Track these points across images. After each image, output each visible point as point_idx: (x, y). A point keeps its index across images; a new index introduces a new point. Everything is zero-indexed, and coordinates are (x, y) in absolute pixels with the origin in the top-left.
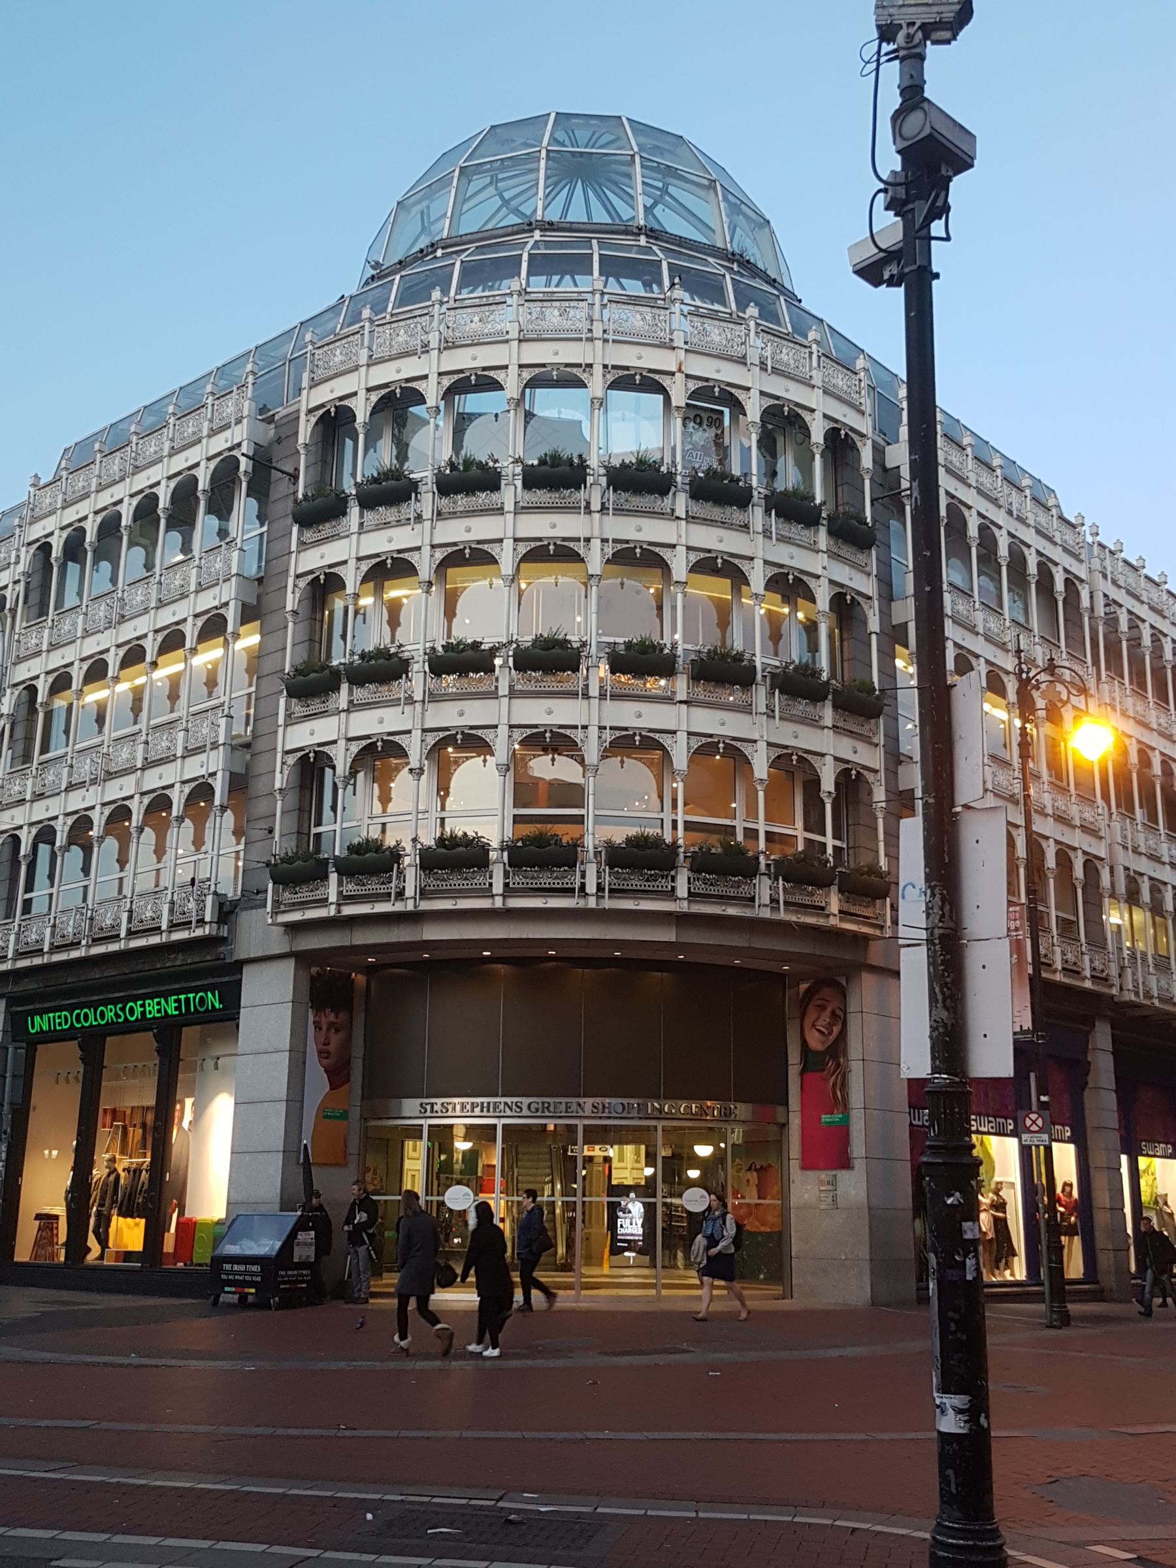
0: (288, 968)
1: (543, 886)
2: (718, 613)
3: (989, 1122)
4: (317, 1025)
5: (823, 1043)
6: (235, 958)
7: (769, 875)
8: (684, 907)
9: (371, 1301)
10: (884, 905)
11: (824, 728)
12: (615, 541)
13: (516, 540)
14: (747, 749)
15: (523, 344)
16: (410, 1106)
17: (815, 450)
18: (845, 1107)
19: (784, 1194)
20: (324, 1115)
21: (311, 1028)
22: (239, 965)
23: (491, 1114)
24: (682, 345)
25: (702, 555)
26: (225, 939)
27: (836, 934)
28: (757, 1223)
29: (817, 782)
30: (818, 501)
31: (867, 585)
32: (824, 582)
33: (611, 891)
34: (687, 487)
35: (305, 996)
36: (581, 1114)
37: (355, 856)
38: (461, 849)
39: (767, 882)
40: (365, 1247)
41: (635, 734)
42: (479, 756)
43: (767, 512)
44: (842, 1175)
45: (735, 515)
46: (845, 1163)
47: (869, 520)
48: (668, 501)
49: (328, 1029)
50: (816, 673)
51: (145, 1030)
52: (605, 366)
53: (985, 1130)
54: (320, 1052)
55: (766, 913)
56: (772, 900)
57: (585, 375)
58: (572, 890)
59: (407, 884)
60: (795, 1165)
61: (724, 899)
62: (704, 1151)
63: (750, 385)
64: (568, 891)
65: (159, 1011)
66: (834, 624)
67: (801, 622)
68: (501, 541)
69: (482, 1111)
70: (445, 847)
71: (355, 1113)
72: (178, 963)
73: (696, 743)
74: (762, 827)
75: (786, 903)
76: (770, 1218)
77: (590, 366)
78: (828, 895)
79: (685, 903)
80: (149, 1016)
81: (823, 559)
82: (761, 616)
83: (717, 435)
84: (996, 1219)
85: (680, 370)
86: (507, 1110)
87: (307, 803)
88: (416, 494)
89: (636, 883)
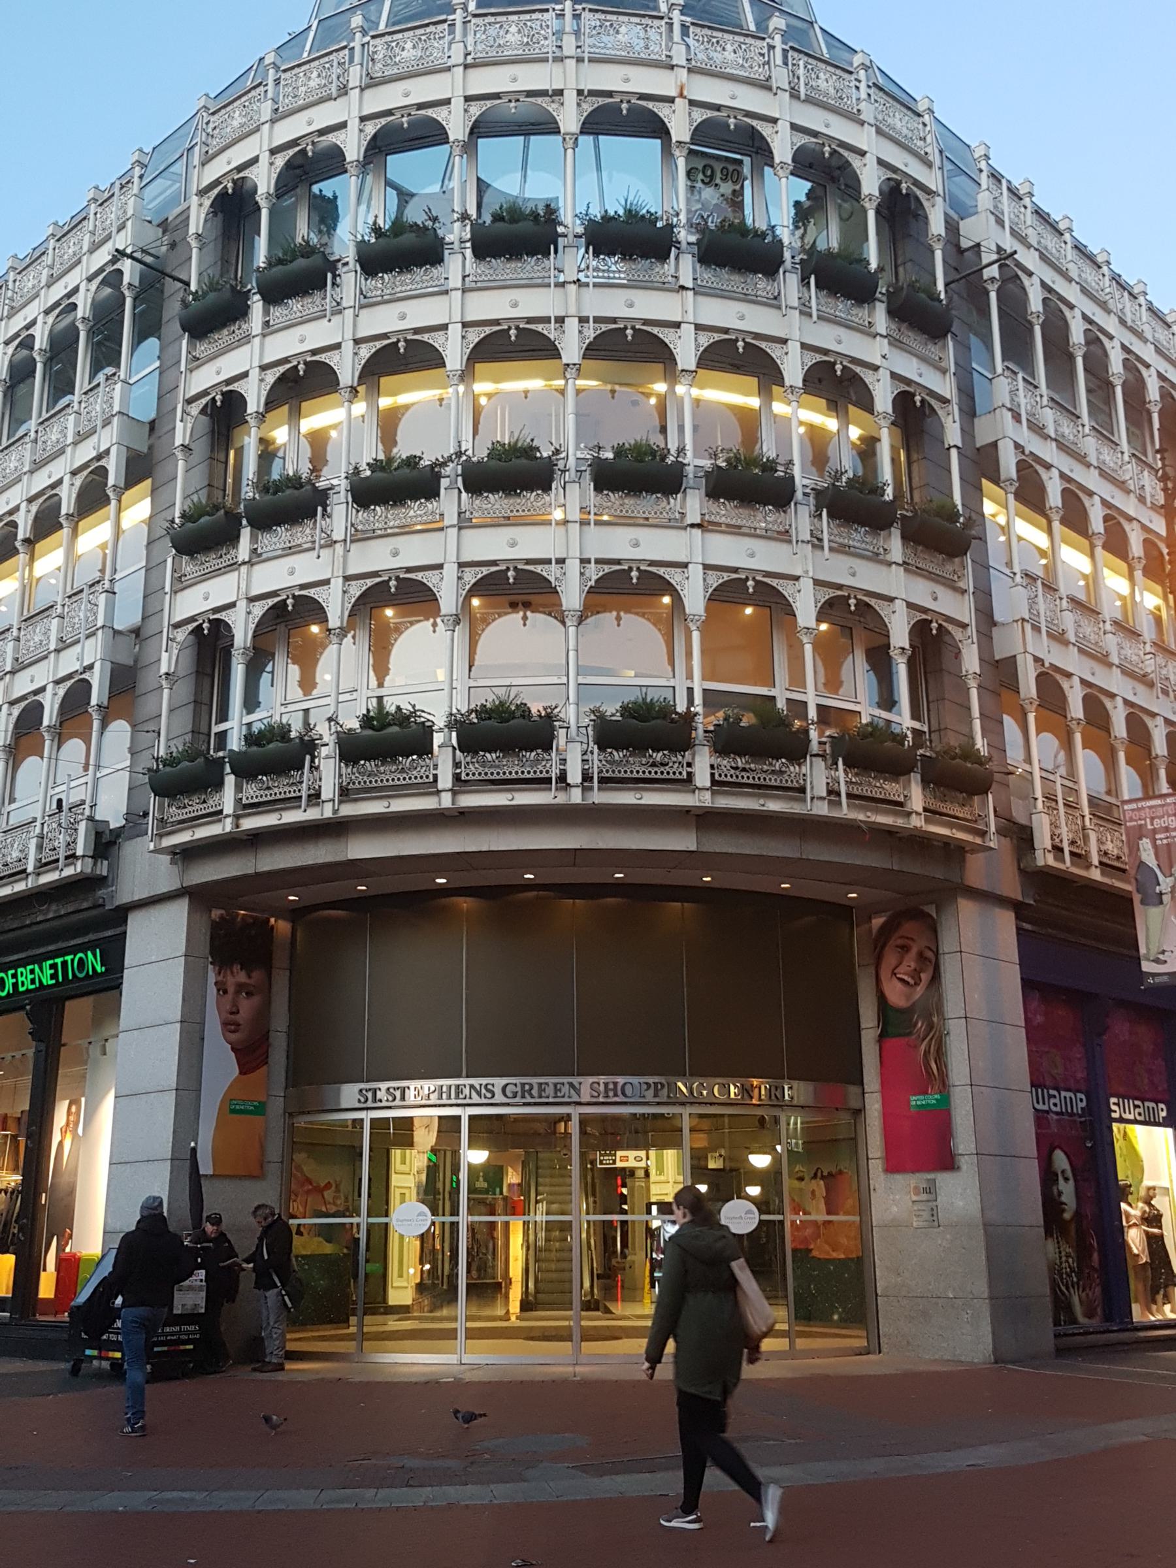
0: (180, 911)
1: (508, 776)
2: (741, 427)
3: (1136, 1107)
4: (222, 988)
5: (908, 997)
6: (117, 903)
7: (823, 756)
8: (705, 800)
9: (289, 1366)
10: (985, 804)
11: (890, 564)
12: (598, 320)
13: (465, 325)
14: (786, 588)
15: (470, 71)
16: (350, 1093)
17: (867, 205)
18: (944, 1085)
19: (863, 1208)
20: (232, 1108)
21: (212, 990)
22: (122, 914)
23: (453, 1101)
24: (684, 63)
25: (717, 337)
26: (105, 878)
27: (918, 843)
28: (827, 1247)
29: (884, 632)
30: (873, 265)
31: (946, 386)
32: (884, 374)
33: (602, 780)
34: (695, 249)
35: (204, 948)
36: (575, 1098)
37: (255, 748)
38: (395, 729)
39: (820, 764)
40: (275, 1291)
41: (631, 569)
42: (427, 619)
43: (805, 282)
44: (944, 1179)
45: (761, 284)
46: (948, 1162)
47: (942, 296)
48: (669, 267)
49: (237, 992)
50: (879, 490)
51: (15, 1010)
52: (580, 92)
53: (1131, 1117)
54: (225, 1024)
55: (822, 809)
56: (830, 792)
57: (554, 106)
58: (548, 781)
59: (323, 783)
60: (876, 1166)
61: (762, 789)
62: (760, 1161)
63: (777, 115)
64: (543, 782)
65: (33, 981)
66: (899, 443)
67: (853, 444)
68: (444, 327)
69: (441, 1098)
70: (373, 728)
71: (277, 1106)
72: (51, 915)
73: (715, 580)
74: (812, 700)
75: (849, 796)
76: (844, 1241)
77: (560, 93)
78: (907, 785)
79: (708, 795)
80: (21, 989)
81: (882, 345)
82: (801, 436)
83: (734, 191)
84: (1149, 1236)
85: (681, 95)
86: (474, 1094)
87: (206, 692)
88: (334, 276)
89: (637, 766)
